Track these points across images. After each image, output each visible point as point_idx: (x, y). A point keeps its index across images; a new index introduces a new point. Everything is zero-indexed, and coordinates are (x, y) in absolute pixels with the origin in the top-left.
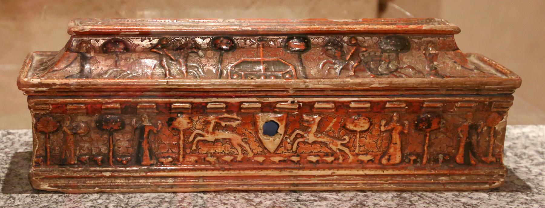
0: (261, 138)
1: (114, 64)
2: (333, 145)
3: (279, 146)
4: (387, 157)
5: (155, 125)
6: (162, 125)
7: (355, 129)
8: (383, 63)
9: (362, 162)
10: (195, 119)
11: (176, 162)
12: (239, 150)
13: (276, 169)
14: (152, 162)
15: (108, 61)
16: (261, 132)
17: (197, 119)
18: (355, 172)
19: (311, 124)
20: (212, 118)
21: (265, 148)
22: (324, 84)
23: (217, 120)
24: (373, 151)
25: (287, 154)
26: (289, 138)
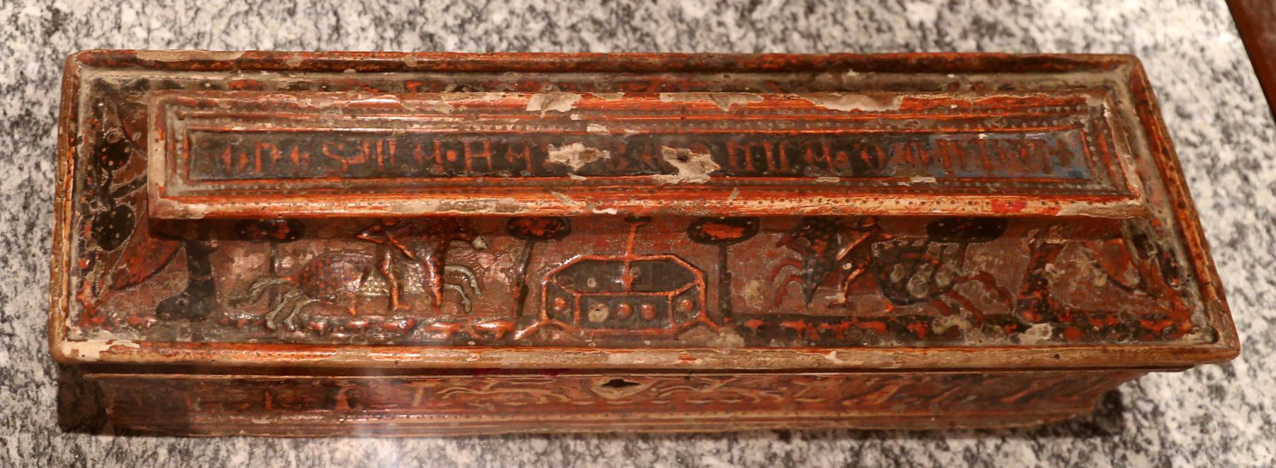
8: (923, 267)
15: (251, 257)
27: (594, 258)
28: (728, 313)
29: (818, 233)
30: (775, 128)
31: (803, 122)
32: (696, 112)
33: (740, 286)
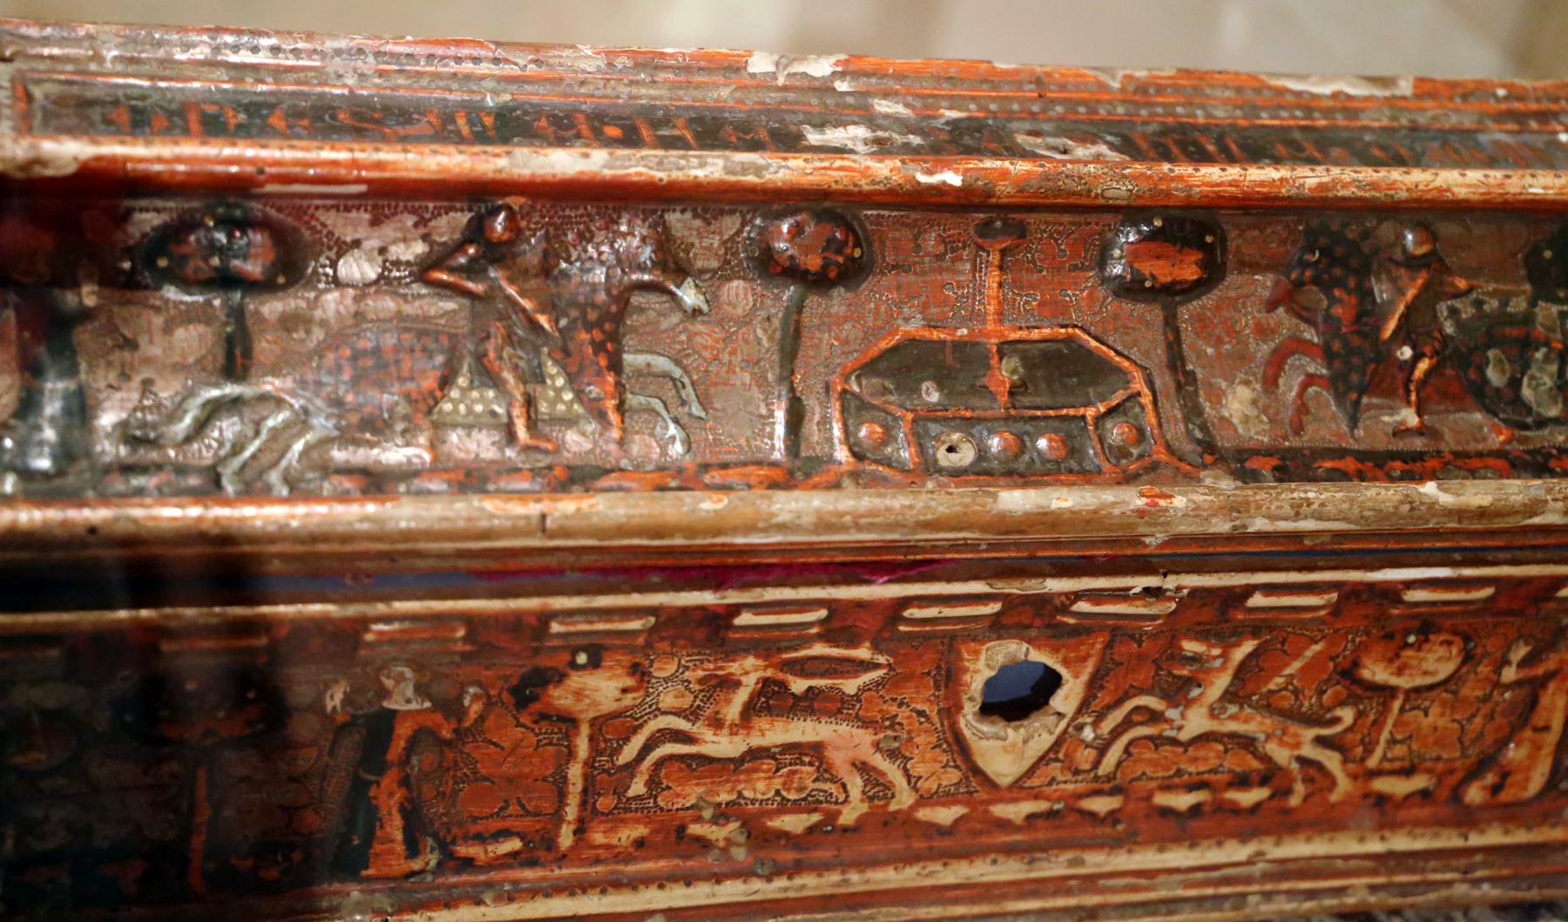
0: (967, 733)
1: (220, 353)
2: (1282, 743)
3: (1041, 758)
4: (1490, 779)
5: (451, 707)
6: (489, 704)
7: (1394, 681)
8: (1539, 355)
9: (1382, 800)
10: (664, 669)
11: (541, 853)
12: (856, 784)
13: (1010, 851)
14: (416, 865)
16: (970, 708)
17: (671, 668)
18: (1347, 845)
19: (1210, 671)
20: (750, 671)
21: (977, 771)
22: (1320, 518)
23: (769, 673)
24: (1438, 759)
25: (1070, 787)
26: (1095, 724)
27: (926, 334)
28: (1208, 446)
29: (1337, 272)
30: (1208, 115)
31: (1254, 110)
32: (1062, 87)
33: (1217, 397)
